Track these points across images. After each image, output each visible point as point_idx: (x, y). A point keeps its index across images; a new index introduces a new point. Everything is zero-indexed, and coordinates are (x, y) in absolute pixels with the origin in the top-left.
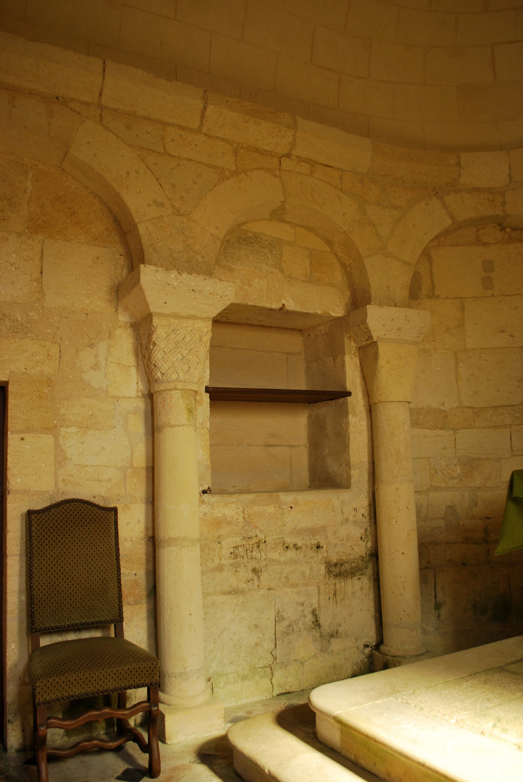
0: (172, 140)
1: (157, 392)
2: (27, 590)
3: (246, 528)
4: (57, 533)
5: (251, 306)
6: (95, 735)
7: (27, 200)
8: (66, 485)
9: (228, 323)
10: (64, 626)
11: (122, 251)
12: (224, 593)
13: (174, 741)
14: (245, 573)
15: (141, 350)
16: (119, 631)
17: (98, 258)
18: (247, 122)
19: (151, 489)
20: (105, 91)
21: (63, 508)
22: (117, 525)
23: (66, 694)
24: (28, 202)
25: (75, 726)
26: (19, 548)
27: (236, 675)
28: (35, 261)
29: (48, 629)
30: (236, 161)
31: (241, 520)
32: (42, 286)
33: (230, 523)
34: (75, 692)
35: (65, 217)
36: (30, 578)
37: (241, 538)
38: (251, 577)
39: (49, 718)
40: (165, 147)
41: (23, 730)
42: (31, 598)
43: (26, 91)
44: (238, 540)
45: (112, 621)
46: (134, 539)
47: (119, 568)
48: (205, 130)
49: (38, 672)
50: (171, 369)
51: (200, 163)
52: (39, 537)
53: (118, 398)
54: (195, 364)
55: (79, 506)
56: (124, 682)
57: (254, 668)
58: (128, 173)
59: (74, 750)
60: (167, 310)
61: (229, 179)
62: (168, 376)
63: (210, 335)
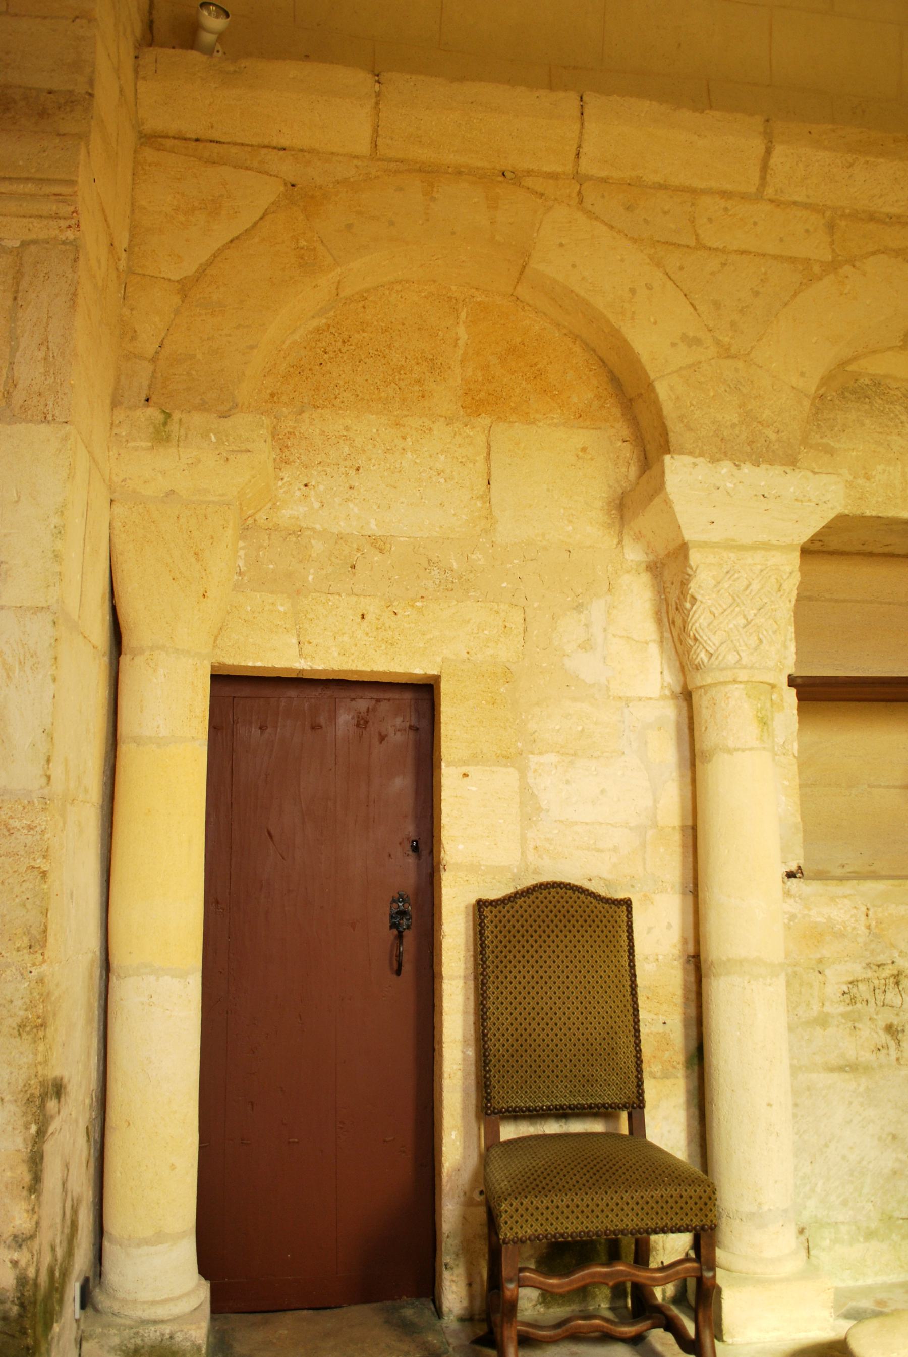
0: (710, 220)
1: (701, 687)
2: (477, 1040)
3: (873, 946)
4: (527, 941)
5: (871, 517)
6: (591, 1308)
7: (459, 358)
8: (540, 857)
9: (824, 552)
10: (542, 1108)
11: (626, 433)
12: (832, 1070)
13: (738, 1340)
14: (871, 1034)
15: (668, 612)
16: (637, 1125)
17: (584, 449)
18: (851, 165)
19: (691, 866)
20: (585, 149)
21: (537, 898)
22: (632, 931)
23: (551, 1230)
24: (462, 361)
25: (567, 1289)
26: (463, 966)
27: (854, 1228)
28: (477, 464)
29: (514, 1111)
30: (832, 243)
31: (862, 930)
32: (490, 506)
33: (841, 935)
34: (567, 1228)
35: (524, 382)
36: (482, 1018)
37: (864, 965)
38: (884, 1041)
39: (521, 1270)
40: (697, 235)
41: (470, 1285)
42: (484, 1055)
43: (450, 170)
44: (857, 970)
45: (625, 1107)
46: (661, 957)
47: (636, 1010)
48: (769, 192)
49: (502, 1185)
50: (725, 646)
51: (764, 255)
52: (497, 947)
53: (627, 701)
54: (770, 633)
55: (564, 895)
56: (652, 1219)
57: (890, 1218)
58: (633, 291)
59: (559, 1331)
60: (715, 535)
61: (821, 279)
62: (720, 658)
63: (796, 578)
